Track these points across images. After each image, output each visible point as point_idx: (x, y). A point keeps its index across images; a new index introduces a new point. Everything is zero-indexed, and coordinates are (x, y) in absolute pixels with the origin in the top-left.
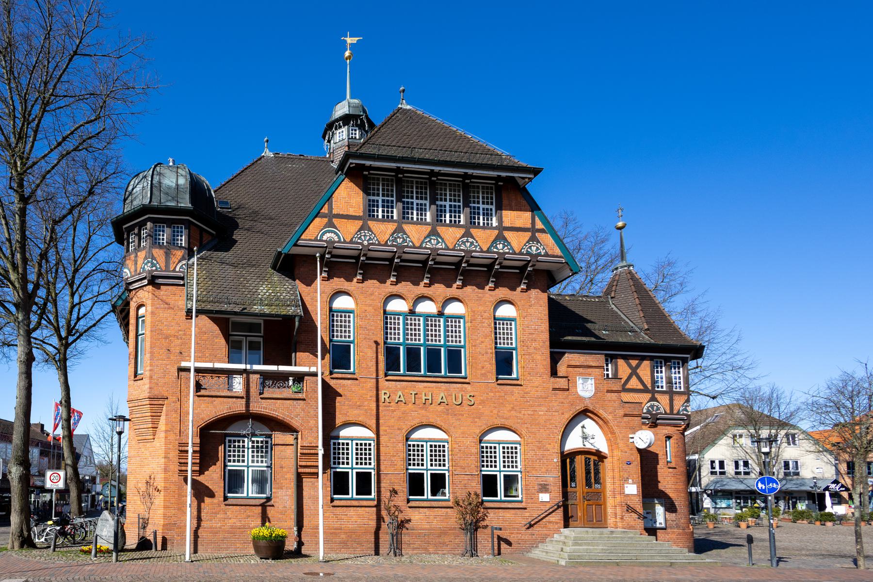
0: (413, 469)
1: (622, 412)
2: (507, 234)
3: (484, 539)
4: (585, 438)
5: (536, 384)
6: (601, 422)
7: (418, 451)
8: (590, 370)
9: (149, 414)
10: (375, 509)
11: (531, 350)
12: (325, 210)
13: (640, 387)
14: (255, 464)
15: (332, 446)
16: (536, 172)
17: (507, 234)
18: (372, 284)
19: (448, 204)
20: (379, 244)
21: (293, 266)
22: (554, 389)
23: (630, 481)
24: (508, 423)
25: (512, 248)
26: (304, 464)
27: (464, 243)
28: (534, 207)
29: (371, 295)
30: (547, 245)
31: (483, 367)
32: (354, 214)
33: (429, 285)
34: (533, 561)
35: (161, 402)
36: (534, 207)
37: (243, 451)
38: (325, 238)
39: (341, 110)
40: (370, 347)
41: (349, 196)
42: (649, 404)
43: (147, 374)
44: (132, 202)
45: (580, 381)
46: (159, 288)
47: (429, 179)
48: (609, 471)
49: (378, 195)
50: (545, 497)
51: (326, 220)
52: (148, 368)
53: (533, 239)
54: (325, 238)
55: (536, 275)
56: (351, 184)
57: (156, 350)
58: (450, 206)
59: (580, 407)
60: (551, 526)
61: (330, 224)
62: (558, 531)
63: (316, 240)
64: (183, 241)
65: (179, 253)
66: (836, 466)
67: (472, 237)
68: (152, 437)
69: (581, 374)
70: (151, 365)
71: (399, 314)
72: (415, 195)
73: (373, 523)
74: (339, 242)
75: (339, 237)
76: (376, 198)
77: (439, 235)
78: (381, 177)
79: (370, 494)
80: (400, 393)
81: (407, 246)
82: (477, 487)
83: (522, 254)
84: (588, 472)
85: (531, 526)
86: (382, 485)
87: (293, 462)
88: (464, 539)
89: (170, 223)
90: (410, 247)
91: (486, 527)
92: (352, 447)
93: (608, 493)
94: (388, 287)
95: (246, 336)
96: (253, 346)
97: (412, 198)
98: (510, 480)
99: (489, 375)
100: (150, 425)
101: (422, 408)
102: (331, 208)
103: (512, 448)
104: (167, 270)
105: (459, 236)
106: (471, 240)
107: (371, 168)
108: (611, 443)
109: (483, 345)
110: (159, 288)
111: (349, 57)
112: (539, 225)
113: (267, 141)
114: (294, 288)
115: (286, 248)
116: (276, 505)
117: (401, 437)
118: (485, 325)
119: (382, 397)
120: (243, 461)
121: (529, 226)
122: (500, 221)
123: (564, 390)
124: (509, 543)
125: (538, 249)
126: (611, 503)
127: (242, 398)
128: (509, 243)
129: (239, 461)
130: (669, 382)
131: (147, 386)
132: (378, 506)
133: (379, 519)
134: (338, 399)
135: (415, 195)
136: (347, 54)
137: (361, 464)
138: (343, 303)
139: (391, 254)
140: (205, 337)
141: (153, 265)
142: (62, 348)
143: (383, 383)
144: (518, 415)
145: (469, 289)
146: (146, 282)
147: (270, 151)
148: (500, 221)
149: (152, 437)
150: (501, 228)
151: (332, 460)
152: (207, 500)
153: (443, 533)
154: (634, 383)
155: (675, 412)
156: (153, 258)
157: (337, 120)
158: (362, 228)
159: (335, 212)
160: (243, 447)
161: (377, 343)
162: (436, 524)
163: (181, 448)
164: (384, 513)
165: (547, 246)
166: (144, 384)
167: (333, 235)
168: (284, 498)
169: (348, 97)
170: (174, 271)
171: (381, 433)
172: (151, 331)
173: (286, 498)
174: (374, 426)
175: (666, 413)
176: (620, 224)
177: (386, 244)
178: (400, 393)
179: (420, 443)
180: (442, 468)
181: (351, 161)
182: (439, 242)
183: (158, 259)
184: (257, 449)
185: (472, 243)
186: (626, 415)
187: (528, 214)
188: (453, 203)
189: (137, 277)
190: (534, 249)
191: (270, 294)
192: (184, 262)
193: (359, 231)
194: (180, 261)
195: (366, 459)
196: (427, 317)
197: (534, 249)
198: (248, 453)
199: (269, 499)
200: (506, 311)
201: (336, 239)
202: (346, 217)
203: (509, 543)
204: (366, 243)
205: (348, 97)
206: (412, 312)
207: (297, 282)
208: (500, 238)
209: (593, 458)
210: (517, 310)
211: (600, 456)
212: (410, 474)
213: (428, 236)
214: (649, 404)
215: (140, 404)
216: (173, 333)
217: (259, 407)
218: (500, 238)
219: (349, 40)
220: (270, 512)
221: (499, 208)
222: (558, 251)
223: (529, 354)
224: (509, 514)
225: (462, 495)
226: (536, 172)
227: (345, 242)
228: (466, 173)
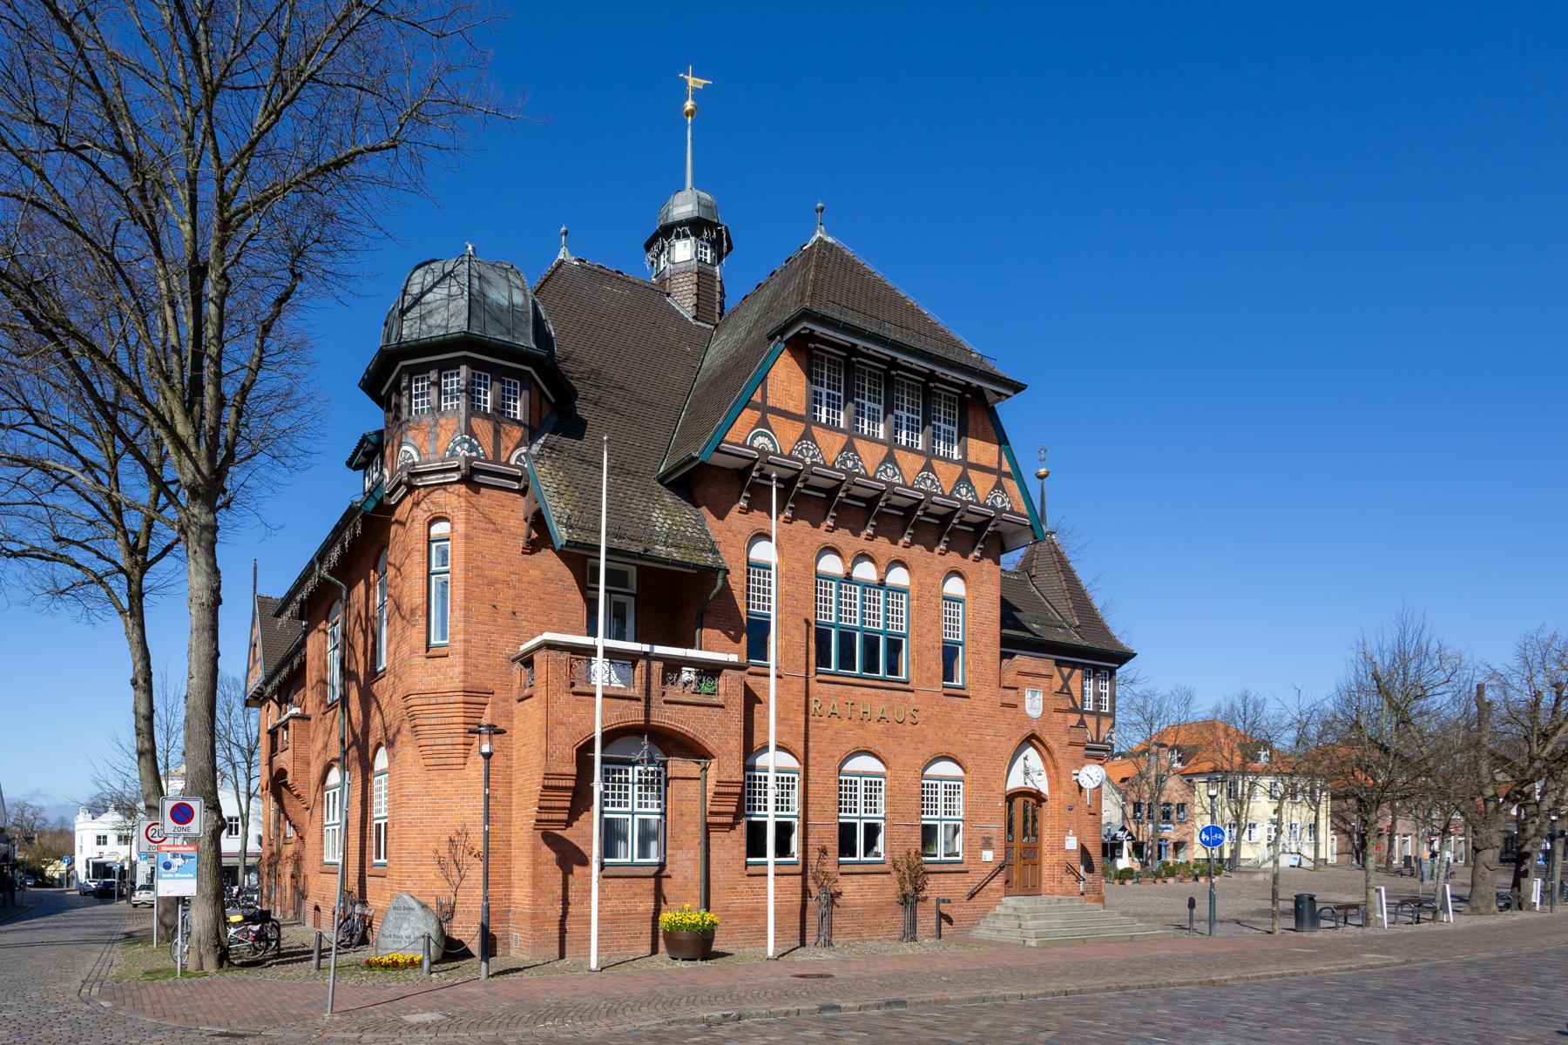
0: (846, 818)
1: (1066, 740)
2: (972, 474)
3: (926, 919)
5: (985, 696)
6: (1045, 753)
8: (1039, 680)
9: (461, 720)
10: (799, 878)
11: (981, 648)
12: (757, 398)
16: (1017, 388)
17: (972, 474)
18: (802, 525)
20: (825, 466)
21: (703, 483)
22: (1004, 705)
24: (954, 751)
25: (975, 496)
26: (715, 809)
28: (1002, 440)
30: (1010, 500)
33: (871, 538)
34: (982, 942)
35: (482, 700)
36: (1002, 440)
37: (626, 788)
39: (683, 207)
40: (797, 627)
41: (789, 379)
43: (459, 647)
44: (422, 318)
45: (1028, 695)
46: (478, 492)
48: (1049, 817)
50: (988, 855)
52: (461, 637)
55: (978, 535)
56: (791, 361)
57: (474, 605)
59: (1027, 732)
60: (991, 894)
61: (763, 423)
62: (999, 902)
64: (518, 410)
65: (517, 433)
66: (1123, 808)
68: (461, 761)
69: (1030, 685)
70: (466, 632)
71: (831, 578)
73: (798, 899)
74: (774, 454)
77: (895, 463)
81: (858, 474)
82: (916, 841)
83: (985, 506)
84: (1026, 821)
85: (972, 895)
86: (810, 841)
87: (697, 805)
88: (899, 918)
89: (499, 374)
91: (925, 899)
93: (1045, 848)
94: (822, 535)
98: (872, 831)
99: (935, 680)
100: (461, 740)
101: (860, 726)
102: (764, 397)
104: (496, 460)
106: (932, 476)
108: (1054, 781)
109: (929, 636)
110: (478, 492)
111: (692, 113)
112: (1006, 468)
113: (566, 233)
114: (700, 521)
115: (700, 451)
116: (674, 875)
117: (833, 770)
119: (813, 706)
120: (626, 805)
121: (995, 466)
122: (964, 451)
124: (950, 921)
126: (1049, 862)
127: (638, 699)
129: (619, 804)
130: (1098, 698)
131: (459, 669)
132: (804, 873)
133: (806, 892)
134: (757, 706)
136: (689, 105)
138: (764, 552)
139: (793, 473)
140: (551, 588)
141: (472, 448)
142: (136, 572)
143: (814, 686)
145: (918, 549)
146: (455, 476)
147: (572, 254)
148: (964, 451)
149: (461, 761)
150: (966, 464)
152: (577, 869)
153: (879, 909)
156: (472, 434)
157: (681, 224)
159: (770, 402)
160: (627, 780)
161: (807, 621)
162: (872, 898)
163: (546, 783)
164: (811, 884)
166: (451, 666)
167: (766, 440)
168: (685, 867)
169: (689, 183)
170: (507, 463)
171: (811, 762)
172: (466, 570)
174: (801, 751)
176: (1043, 471)
177: (833, 468)
178: (834, 702)
181: (805, 324)
183: (480, 437)
184: (645, 784)
186: (1071, 744)
187: (995, 448)
189: (437, 465)
191: (671, 528)
192: (524, 450)
194: (517, 447)
196: (866, 586)
198: (633, 791)
199: (662, 866)
200: (955, 587)
202: (785, 416)
203: (950, 921)
204: (808, 461)
205: (689, 183)
206: (848, 577)
207: (704, 510)
208: (964, 479)
209: (1032, 801)
210: (967, 588)
211: (1039, 798)
212: (841, 825)
215: (441, 700)
216: (501, 576)
217: (664, 717)
218: (964, 479)
219: (693, 82)
220: (667, 886)
221: (963, 433)
222: (1023, 509)
223: (979, 653)
225: (900, 853)
226: (1017, 388)
227: (782, 455)
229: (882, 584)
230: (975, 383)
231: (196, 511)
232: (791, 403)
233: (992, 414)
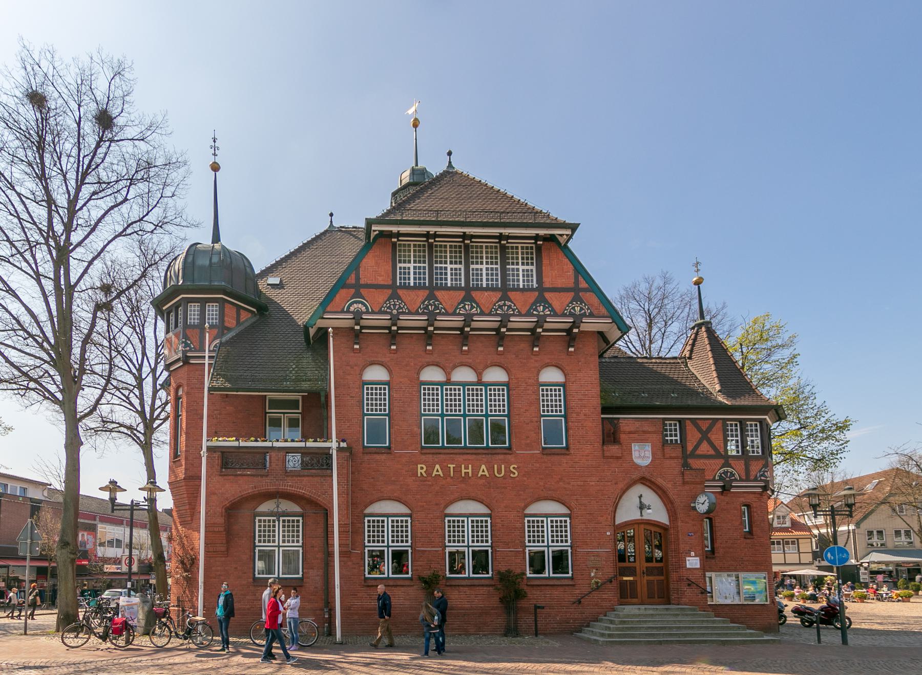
2: (548, 295)
4: (642, 507)
7: (458, 527)
8: (648, 435)
11: (582, 417)
13: (712, 452)
14: (475, 544)
15: (366, 524)
17: (548, 295)
19: (412, 265)
23: (693, 554)
25: (553, 310)
27: (500, 307)
29: (406, 365)
31: (528, 437)
32: (382, 283)
38: (352, 309)
42: (721, 471)
45: (635, 447)
47: (535, 243)
49: (409, 262)
51: (353, 291)
53: (577, 299)
54: (352, 309)
58: (487, 269)
63: (342, 312)
67: (438, 301)
69: (637, 441)
72: (448, 260)
74: (367, 312)
75: (367, 308)
76: (407, 265)
77: (399, 298)
78: (412, 243)
79: (568, 573)
80: (437, 467)
90: (443, 314)
92: (468, 523)
95: (284, 413)
96: (293, 423)
97: (517, 264)
102: (358, 278)
103: (561, 521)
105: (494, 300)
106: (508, 303)
107: (399, 235)
118: (530, 392)
123: (618, 458)
125: (581, 309)
128: (550, 305)
135: (448, 260)
137: (398, 541)
144: (566, 486)
151: (527, 539)
154: (705, 448)
155: (752, 478)
158: (429, 298)
159: (362, 282)
165: (592, 305)
173: (317, 578)
175: (741, 480)
179: (461, 519)
180: (381, 544)
182: (472, 307)
185: (509, 307)
188: (490, 266)
190: (577, 309)
193: (388, 300)
195: (459, 536)
197: (577, 309)
201: (364, 309)
204: (395, 312)
213: (462, 301)
214: (721, 471)
224: (556, 593)
226: (574, 227)
227: (373, 312)
228: (537, 235)
229: (480, 382)
230: (542, 232)
231: (780, 473)
232: (380, 279)
233: (565, 248)
